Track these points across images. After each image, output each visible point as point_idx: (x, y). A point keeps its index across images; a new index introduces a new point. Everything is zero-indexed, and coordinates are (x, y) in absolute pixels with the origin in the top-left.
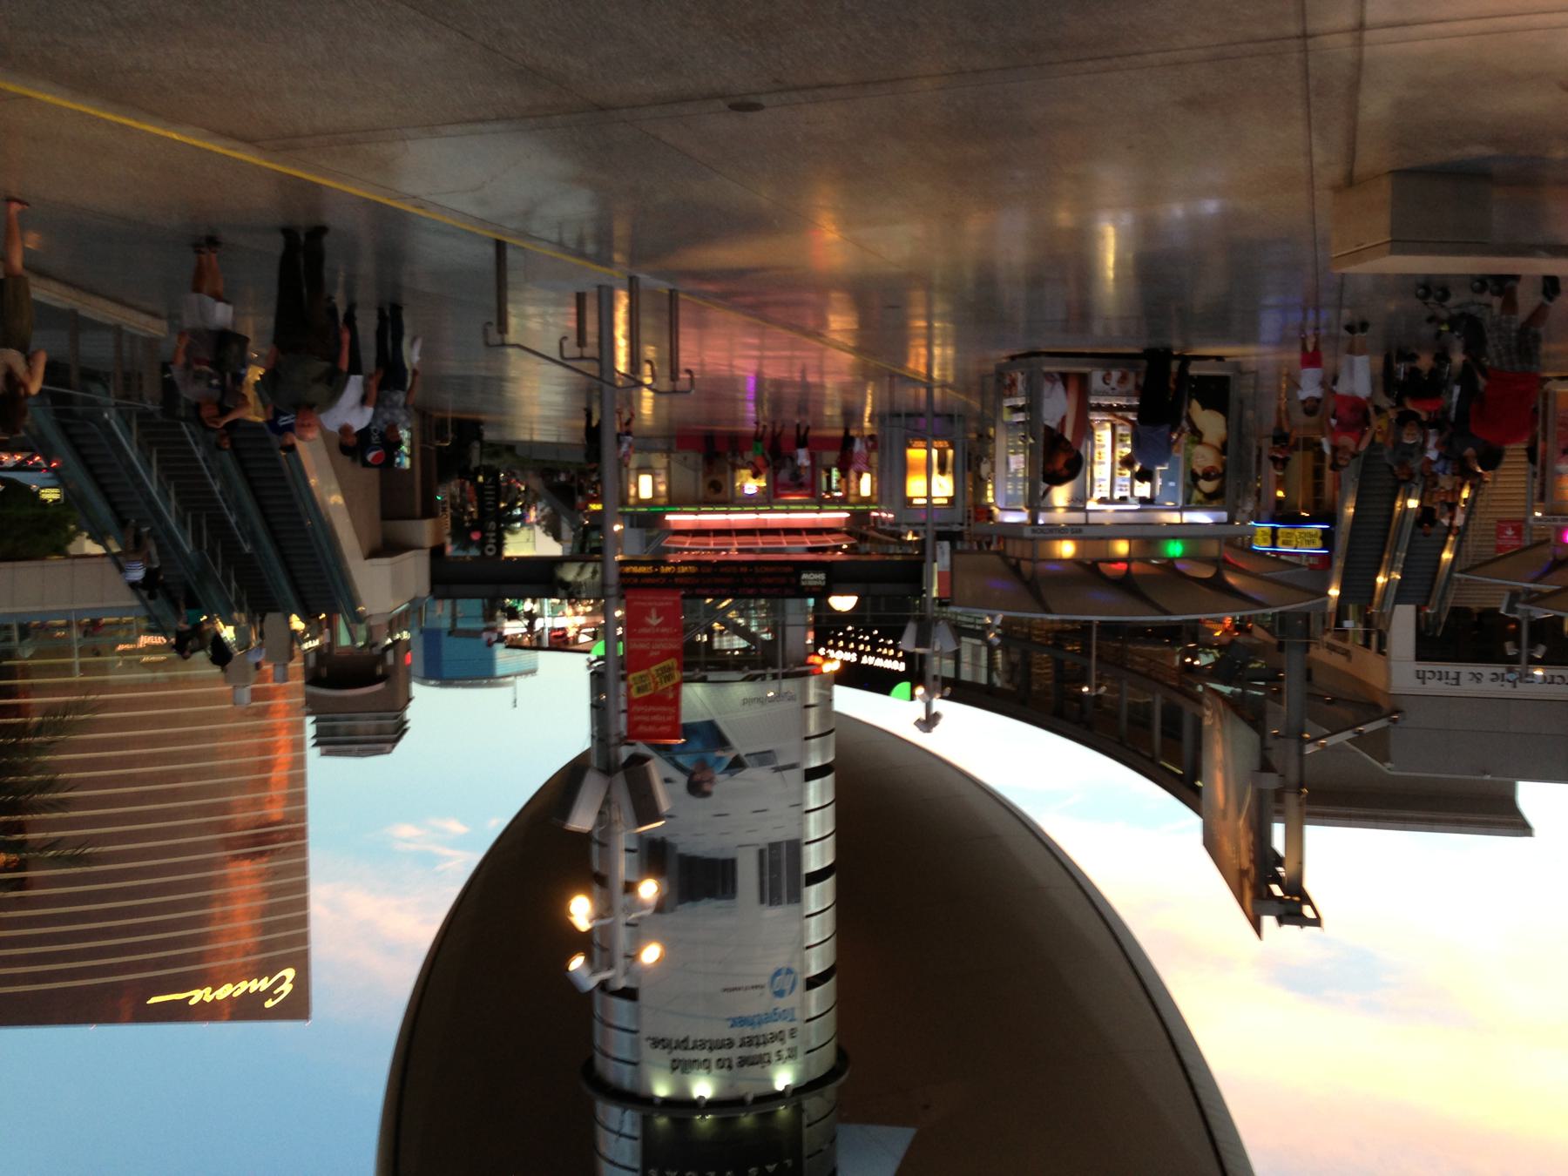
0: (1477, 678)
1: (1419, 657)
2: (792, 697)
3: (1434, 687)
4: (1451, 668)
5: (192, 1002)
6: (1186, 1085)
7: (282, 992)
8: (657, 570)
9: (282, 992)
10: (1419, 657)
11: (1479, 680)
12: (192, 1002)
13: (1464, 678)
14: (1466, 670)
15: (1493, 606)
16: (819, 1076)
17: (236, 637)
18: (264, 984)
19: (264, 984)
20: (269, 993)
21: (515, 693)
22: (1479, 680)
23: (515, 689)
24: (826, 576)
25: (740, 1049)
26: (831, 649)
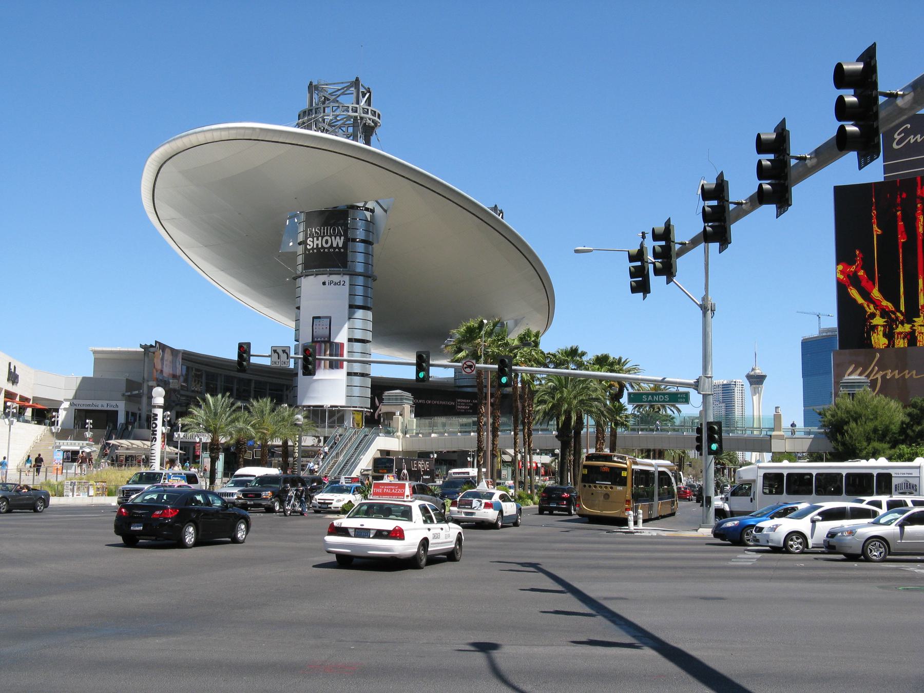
0: (102, 406)
1: (117, 412)
2: (740, 487)
3: (113, 403)
4: (109, 408)
7: (898, 135)
8: (721, 203)
9: (898, 135)
10: (117, 412)
11: (102, 405)
13: (100, 406)
14: (105, 408)
15: (632, 432)
16: (599, 647)
17: (164, 404)
18: (912, 139)
19: (912, 139)
20: (907, 133)
21: (819, 323)
22: (102, 405)
23: (820, 327)
24: (902, 348)
25: (329, 130)
26: (902, 444)
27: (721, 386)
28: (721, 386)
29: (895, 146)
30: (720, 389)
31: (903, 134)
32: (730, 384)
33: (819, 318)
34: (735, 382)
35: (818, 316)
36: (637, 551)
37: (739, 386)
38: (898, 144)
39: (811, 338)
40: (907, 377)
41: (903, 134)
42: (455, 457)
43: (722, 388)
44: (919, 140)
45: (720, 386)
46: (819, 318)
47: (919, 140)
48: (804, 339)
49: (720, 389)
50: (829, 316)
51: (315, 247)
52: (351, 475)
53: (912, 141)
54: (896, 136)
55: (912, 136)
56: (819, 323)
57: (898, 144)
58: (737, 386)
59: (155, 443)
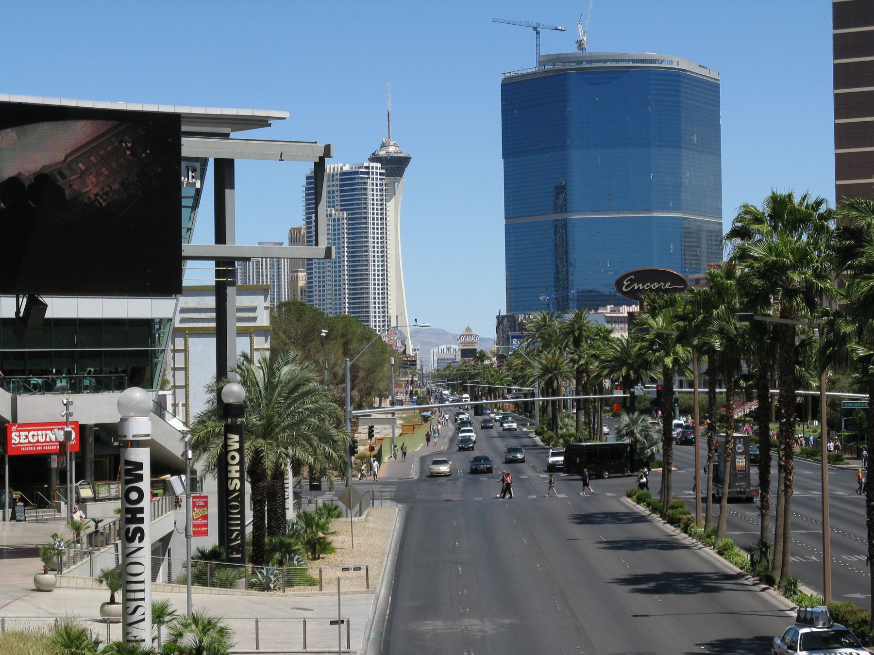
7: (627, 282)
9: (627, 282)
20: (632, 282)
21: (538, 45)
23: (538, 53)
27: (338, 177)
28: (338, 177)
29: (624, 289)
30: (335, 183)
32: (357, 173)
33: (538, 33)
34: (368, 168)
35: (535, 29)
36: (162, 505)
37: (375, 176)
38: (626, 288)
39: (522, 76)
40: (641, 285)
42: (609, 519)
43: (341, 186)
44: (636, 285)
45: (336, 177)
46: (538, 33)
47: (636, 285)
48: (506, 79)
49: (335, 183)
50: (556, 29)
52: (832, 515)
54: (625, 283)
56: (538, 45)
57: (626, 288)
58: (371, 176)
59: (140, 545)
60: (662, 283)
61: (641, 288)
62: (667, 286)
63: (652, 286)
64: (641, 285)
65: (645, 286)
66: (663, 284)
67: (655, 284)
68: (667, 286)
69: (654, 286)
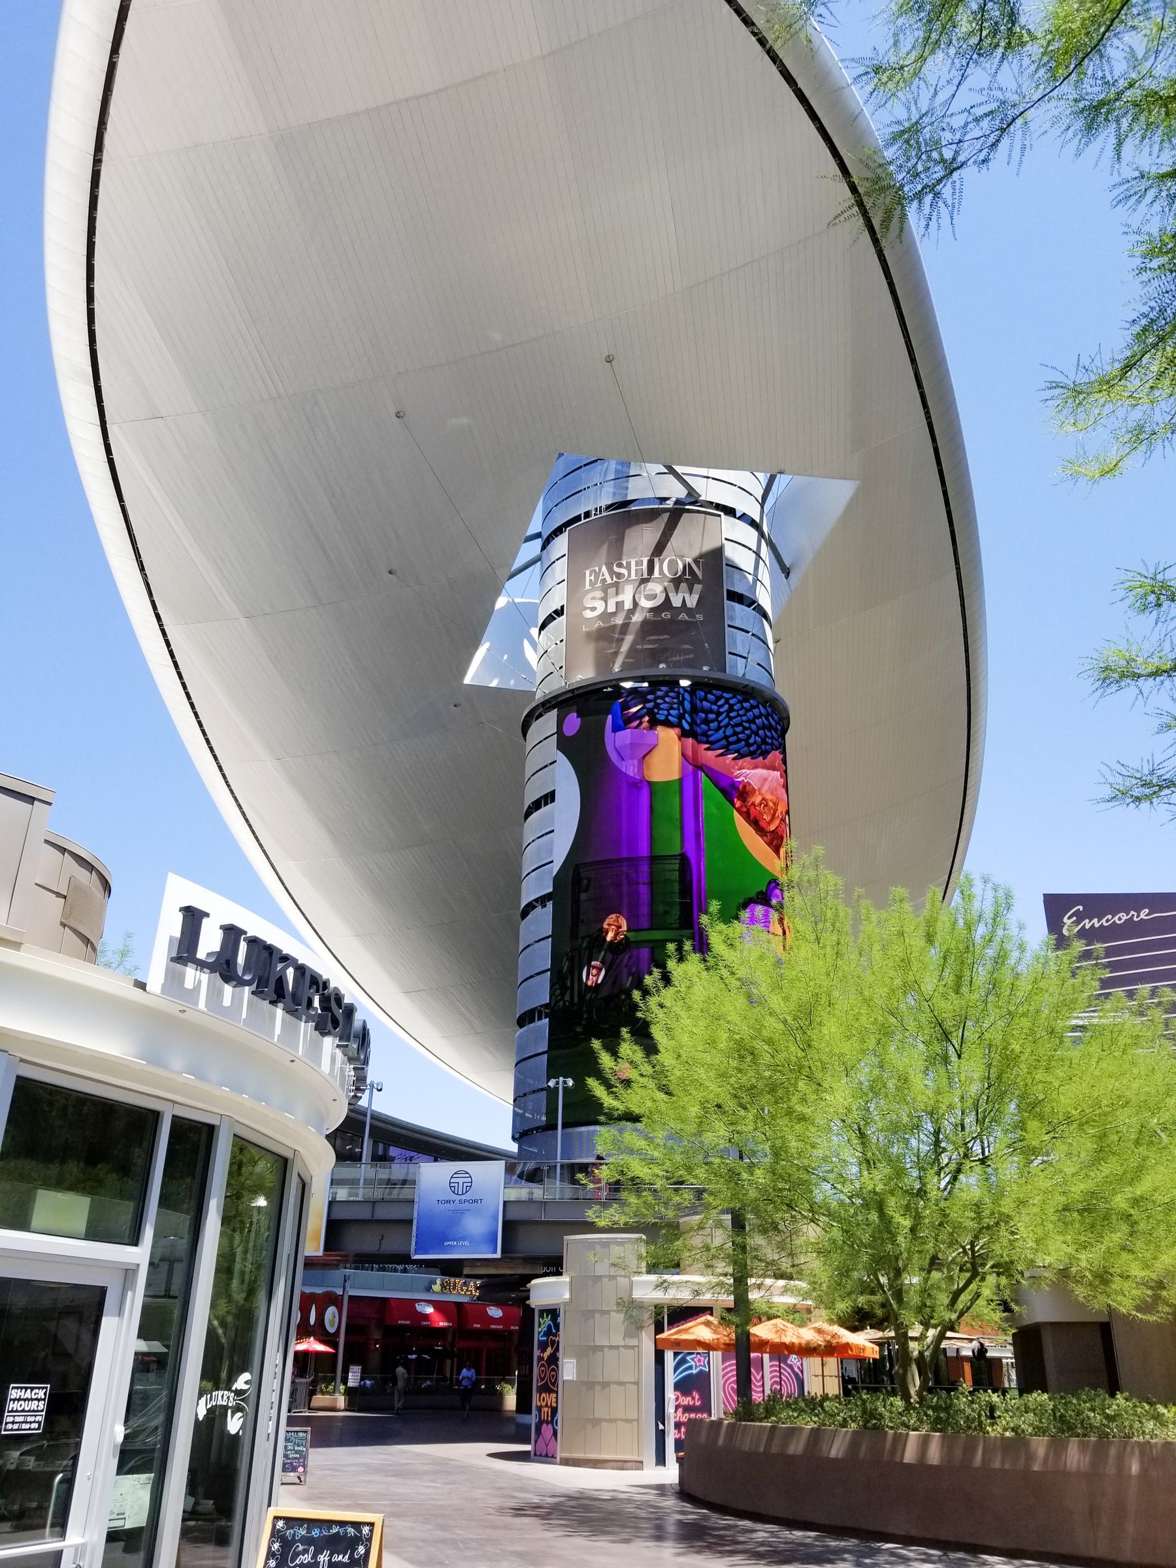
5: (1147, 911)
6: (231, 783)
12: (1147, 911)
18: (1087, 924)
19: (1087, 924)
20: (1080, 917)
31: (1075, 918)
41: (1075, 918)
51: (612, 608)
53: (1087, 927)
54: (1065, 920)
55: (1087, 921)
60: (1132, 913)
61: (1097, 925)
62: (1142, 916)
63: (1116, 918)
64: (1095, 920)
65: (1104, 921)
66: (1136, 914)
67: (1121, 915)
68: (1142, 916)
69: (1120, 919)
